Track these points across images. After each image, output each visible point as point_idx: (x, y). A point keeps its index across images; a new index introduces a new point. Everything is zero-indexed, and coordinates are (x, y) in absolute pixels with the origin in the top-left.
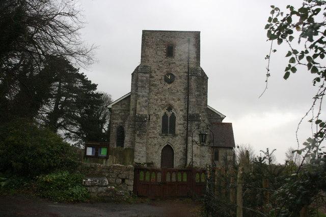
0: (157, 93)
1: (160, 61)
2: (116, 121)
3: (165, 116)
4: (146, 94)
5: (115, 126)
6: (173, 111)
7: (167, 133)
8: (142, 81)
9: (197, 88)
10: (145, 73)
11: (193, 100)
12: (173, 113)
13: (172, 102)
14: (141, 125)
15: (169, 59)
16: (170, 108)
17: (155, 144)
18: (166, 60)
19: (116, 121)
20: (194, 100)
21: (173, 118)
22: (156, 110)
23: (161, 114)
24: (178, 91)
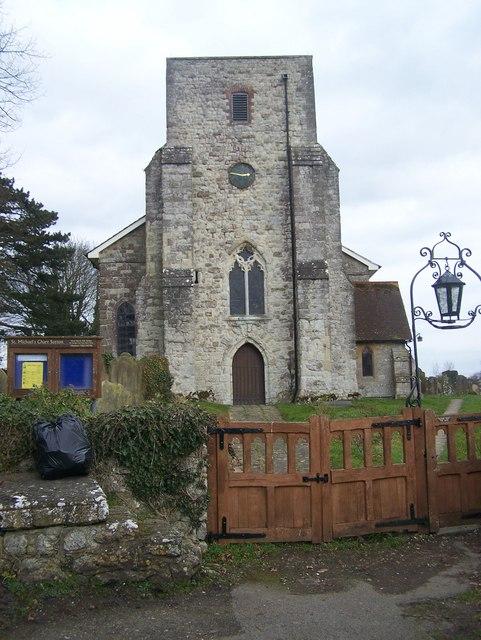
0: (214, 214)
1: (215, 135)
2: (113, 291)
3: (236, 274)
4: (184, 218)
5: (111, 304)
6: (255, 256)
7: (245, 313)
8: (173, 186)
9: (315, 195)
10: (178, 164)
11: (303, 225)
12: (256, 262)
13: (251, 236)
14: (177, 296)
15: (241, 129)
16: (248, 250)
17: (216, 345)
18: (230, 129)
19: (113, 291)
20: (307, 226)
21: (257, 274)
22: (211, 256)
23: (227, 266)
24: (264, 207)
